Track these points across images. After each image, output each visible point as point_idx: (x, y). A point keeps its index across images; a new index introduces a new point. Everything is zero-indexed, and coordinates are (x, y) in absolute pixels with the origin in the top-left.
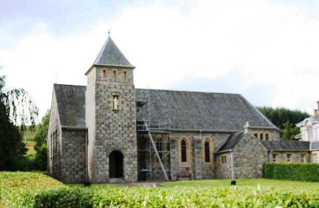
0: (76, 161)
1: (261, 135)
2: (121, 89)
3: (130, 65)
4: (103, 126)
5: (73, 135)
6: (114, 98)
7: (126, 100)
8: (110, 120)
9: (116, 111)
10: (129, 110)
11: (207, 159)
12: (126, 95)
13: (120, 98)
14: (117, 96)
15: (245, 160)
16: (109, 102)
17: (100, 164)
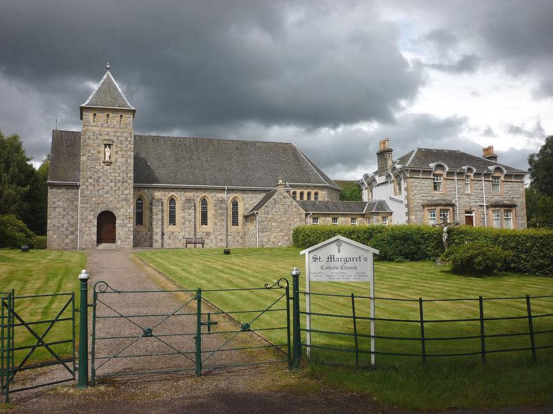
6: (105, 148)
7: (122, 150)
8: (100, 174)
9: (109, 163)
11: (235, 223)
13: (114, 147)
14: (110, 145)
15: (274, 224)
16: (99, 152)
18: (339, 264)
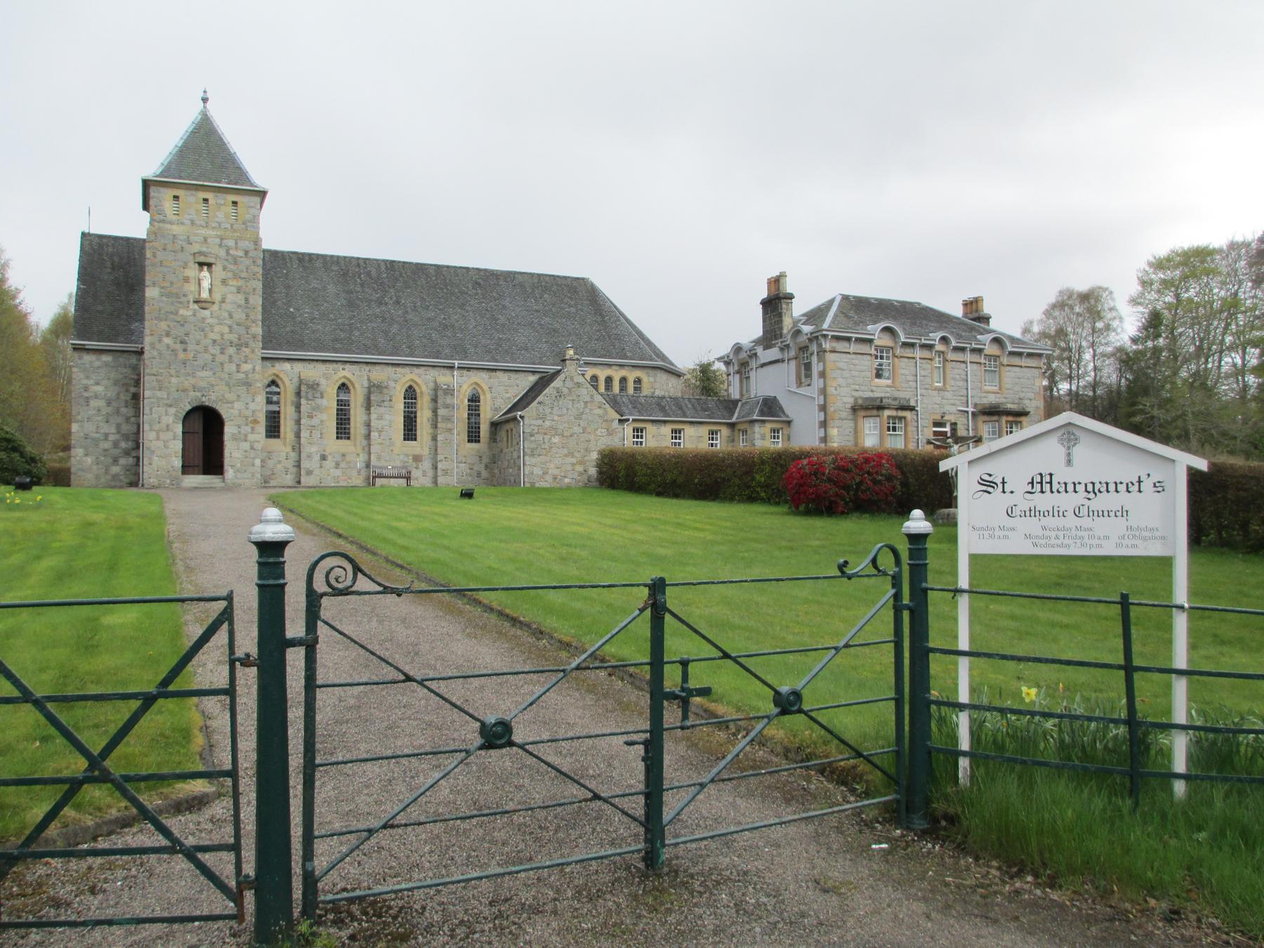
0: (113, 430)
1: (609, 380)
2: (220, 246)
3: (252, 185)
4: (167, 340)
5: (107, 364)
10: (243, 302)
11: (473, 436)
12: (236, 263)
15: (556, 440)
17: (158, 438)
18: (1069, 501)
